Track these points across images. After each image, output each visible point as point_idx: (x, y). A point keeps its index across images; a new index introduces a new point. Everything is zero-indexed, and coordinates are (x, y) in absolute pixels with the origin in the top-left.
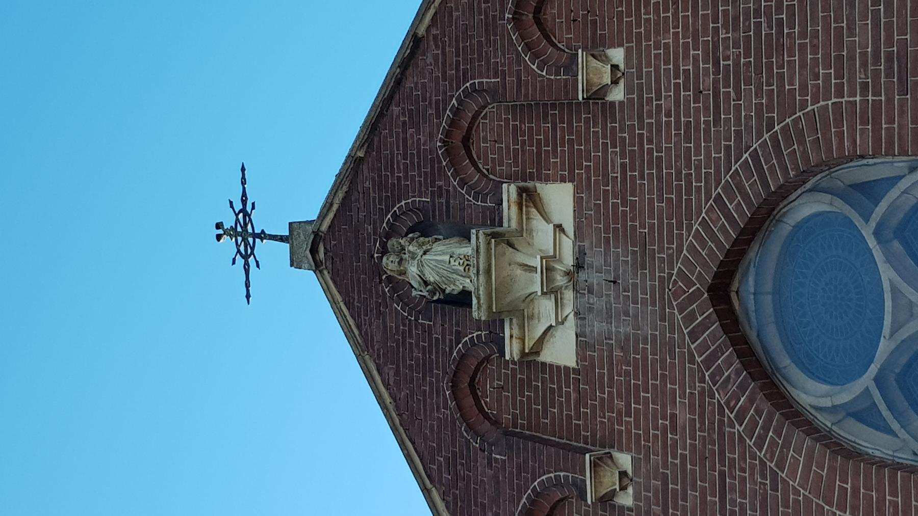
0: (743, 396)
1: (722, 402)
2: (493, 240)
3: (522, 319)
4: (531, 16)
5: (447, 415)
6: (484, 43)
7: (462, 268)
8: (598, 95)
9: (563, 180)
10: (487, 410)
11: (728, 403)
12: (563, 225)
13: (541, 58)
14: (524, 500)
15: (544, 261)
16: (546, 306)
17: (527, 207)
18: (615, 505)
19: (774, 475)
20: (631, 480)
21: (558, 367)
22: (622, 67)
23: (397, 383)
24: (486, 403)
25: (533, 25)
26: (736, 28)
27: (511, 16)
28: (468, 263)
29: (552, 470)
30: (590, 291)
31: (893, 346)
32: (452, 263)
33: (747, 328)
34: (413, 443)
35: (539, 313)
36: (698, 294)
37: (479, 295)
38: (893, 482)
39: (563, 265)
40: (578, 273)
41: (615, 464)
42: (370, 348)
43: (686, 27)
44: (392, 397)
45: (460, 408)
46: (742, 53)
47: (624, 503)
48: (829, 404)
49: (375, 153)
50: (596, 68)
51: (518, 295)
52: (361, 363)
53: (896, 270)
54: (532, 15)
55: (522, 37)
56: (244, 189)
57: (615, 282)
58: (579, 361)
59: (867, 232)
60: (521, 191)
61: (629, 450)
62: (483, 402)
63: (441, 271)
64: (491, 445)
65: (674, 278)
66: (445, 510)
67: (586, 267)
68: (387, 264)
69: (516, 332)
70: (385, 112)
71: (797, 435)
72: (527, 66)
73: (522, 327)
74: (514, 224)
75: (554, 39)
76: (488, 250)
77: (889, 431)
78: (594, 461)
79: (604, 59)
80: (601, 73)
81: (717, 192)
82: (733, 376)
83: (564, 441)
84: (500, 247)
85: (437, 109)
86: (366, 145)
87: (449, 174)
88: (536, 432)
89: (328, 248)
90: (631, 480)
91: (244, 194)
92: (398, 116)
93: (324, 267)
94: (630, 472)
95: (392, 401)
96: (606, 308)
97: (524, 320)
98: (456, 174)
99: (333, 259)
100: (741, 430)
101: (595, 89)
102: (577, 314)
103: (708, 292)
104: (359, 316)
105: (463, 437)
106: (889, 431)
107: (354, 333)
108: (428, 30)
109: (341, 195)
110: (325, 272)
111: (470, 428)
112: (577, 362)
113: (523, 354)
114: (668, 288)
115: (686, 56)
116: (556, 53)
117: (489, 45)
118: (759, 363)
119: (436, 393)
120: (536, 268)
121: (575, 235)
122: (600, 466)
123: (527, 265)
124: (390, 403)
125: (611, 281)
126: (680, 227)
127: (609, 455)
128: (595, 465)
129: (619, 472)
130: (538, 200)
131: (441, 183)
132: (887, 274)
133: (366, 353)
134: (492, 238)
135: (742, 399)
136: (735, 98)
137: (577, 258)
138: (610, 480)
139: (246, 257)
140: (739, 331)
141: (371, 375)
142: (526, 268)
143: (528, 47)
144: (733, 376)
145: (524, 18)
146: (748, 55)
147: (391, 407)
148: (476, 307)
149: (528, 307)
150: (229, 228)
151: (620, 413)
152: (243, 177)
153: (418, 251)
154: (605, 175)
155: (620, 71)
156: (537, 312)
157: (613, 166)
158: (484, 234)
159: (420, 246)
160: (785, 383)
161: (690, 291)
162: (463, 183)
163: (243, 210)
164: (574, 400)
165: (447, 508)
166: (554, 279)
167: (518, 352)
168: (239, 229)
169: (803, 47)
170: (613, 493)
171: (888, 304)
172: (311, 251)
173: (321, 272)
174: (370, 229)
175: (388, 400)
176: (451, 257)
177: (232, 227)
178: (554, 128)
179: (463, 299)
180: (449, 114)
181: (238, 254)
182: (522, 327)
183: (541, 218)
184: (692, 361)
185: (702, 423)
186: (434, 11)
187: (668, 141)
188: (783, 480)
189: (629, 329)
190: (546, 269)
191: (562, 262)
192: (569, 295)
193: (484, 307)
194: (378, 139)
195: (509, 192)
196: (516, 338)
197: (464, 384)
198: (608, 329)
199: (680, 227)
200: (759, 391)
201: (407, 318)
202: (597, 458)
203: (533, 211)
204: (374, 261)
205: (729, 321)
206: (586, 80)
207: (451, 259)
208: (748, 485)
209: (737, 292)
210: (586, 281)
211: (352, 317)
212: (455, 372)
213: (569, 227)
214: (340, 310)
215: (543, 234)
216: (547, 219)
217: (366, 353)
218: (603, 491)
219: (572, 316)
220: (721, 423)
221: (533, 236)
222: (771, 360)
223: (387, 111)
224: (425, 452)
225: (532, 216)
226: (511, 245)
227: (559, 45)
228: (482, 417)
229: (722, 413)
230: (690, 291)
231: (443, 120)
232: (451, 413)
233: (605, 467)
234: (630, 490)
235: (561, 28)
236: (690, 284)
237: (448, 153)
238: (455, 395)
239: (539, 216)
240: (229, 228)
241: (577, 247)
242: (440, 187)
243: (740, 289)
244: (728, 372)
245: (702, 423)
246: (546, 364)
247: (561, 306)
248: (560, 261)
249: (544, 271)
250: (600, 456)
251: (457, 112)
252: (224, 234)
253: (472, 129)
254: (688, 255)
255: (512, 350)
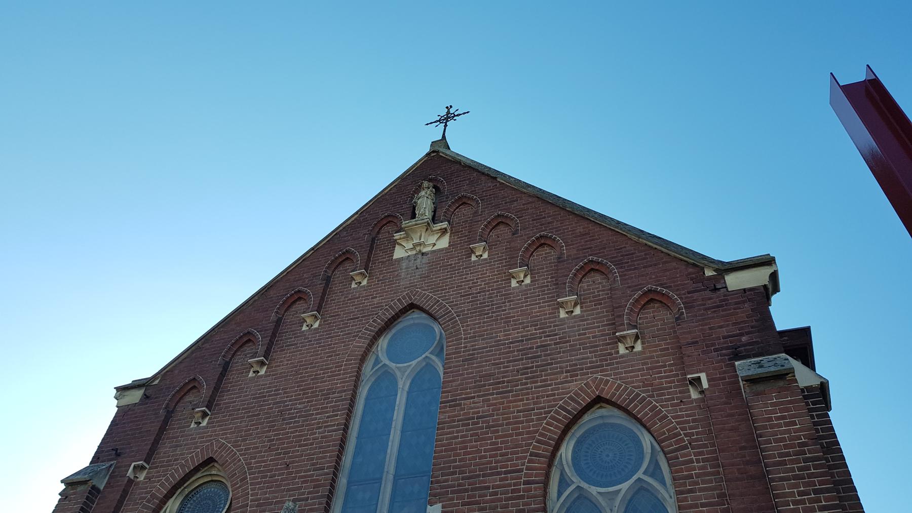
4: (500, 220)
7: (421, 213)
8: (472, 251)
9: (450, 243)
14: (353, 249)
16: (409, 245)
19: (357, 336)
22: (482, 258)
23: (391, 194)
26: (489, 298)
30: (415, 260)
31: (394, 368)
33: (403, 317)
36: (411, 299)
38: (352, 376)
43: (491, 279)
48: (379, 349)
53: (415, 365)
55: (492, 220)
57: (417, 268)
59: (427, 354)
60: (445, 229)
64: (370, 234)
69: (402, 236)
71: (367, 341)
73: (404, 238)
74: (434, 229)
76: (423, 223)
77: (372, 369)
94: (361, 285)
102: (409, 256)
106: (372, 369)
109: (450, 158)
113: (396, 240)
115: (482, 281)
126: (431, 289)
132: (414, 363)
139: (439, 121)
147: (383, 193)
151: (378, 278)
152: (465, 113)
154: (449, 258)
160: (384, 336)
163: (455, 116)
171: (406, 365)
172: (433, 151)
179: (413, 216)
182: (404, 238)
184: (392, 301)
185: (374, 308)
188: (355, 339)
189: (403, 276)
192: (414, 252)
195: (445, 225)
199: (431, 289)
209: (413, 312)
213: (435, 248)
214: (414, 167)
215: (432, 239)
216: (436, 241)
218: (354, 277)
220: (373, 314)
222: (395, 326)
226: (427, 230)
234: (356, 286)
235: (496, 232)
245: (374, 308)
248: (424, 247)
251: (472, 199)
255: (397, 236)
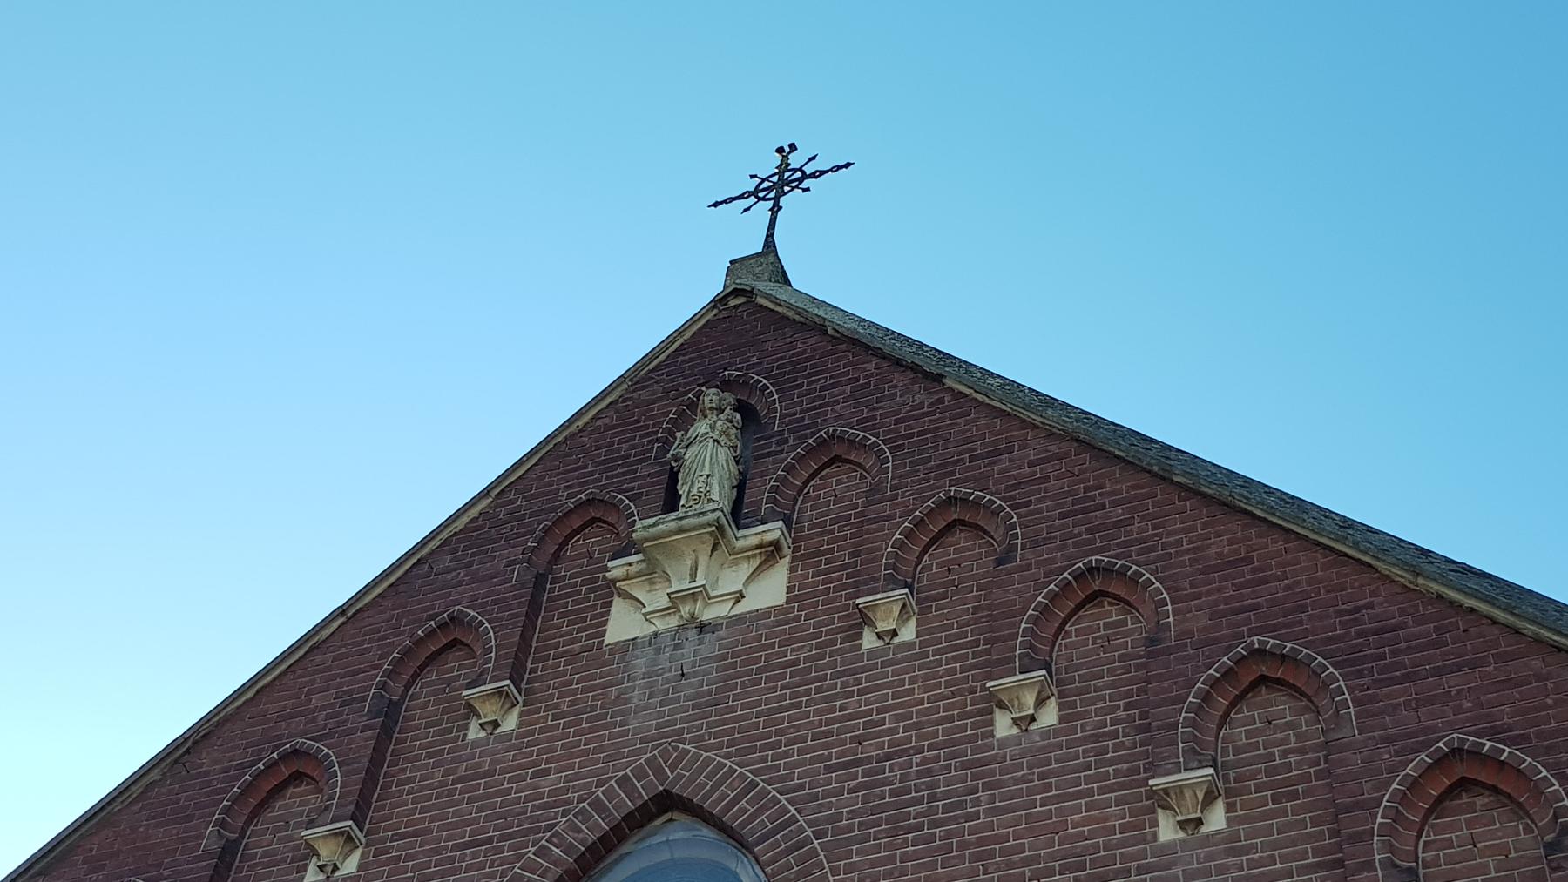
0: (561, 851)
1: (557, 828)
2: (714, 528)
3: (648, 572)
4: (956, 516)
5: (561, 501)
6: (929, 465)
7: (695, 491)
9: (790, 590)
10: (571, 543)
11: (557, 834)
12: (744, 599)
13: (906, 541)
15: (701, 589)
17: (760, 553)
18: (469, 719)
20: (491, 734)
21: (605, 623)
22: (896, 640)
23: (597, 431)
24: (578, 540)
25: (945, 521)
26: (920, 775)
27: (952, 494)
28: (703, 497)
29: (498, 642)
32: (701, 479)
33: (635, 839)
34: (536, 464)
35: (656, 590)
37: (658, 525)
39: (702, 608)
40: (696, 627)
41: (505, 713)
42: (635, 387)
44: (584, 426)
45: (567, 514)
46: (895, 786)
47: (471, 729)
49: (830, 348)
50: (891, 612)
51: (666, 566)
52: (315, 630)
54: (957, 518)
56: (827, 172)
57: (683, 675)
58: (610, 647)
60: (776, 544)
61: (520, 725)
62: (579, 536)
63: (695, 466)
65: (681, 746)
66: (470, 518)
67: (700, 636)
68: (709, 395)
69: (634, 569)
70: (870, 352)
72: (899, 524)
73: (640, 574)
74: (740, 544)
75: (932, 549)
76: (702, 526)
78: (502, 691)
79: (905, 617)
80: (888, 617)
81: (760, 782)
82: (581, 836)
83: (534, 645)
84: (708, 537)
85: (867, 419)
86: (839, 336)
87: (799, 450)
88: (545, 608)
89: (740, 309)
90: (491, 734)
91: (823, 173)
92: (865, 370)
93: (721, 308)
94: (499, 731)
95: (580, 427)
96: (659, 669)
97: (647, 575)
98: (799, 458)
99: (728, 317)
100: (530, 855)
101: (870, 614)
102: (656, 634)
103: (664, 790)
104: (667, 366)
105: (539, 524)
107: (650, 363)
108: (951, 389)
109: (790, 314)
110: (715, 312)
111: (547, 530)
112: (609, 645)
113: (614, 581)
114: (672, 741)
115: (898, 718)
116: (914, 558)
117: (926, 472)
118: (600, 859)
119: (584, 482)
120: (695, 581)
121: (734, 616)
122: (501, 697)
123: (696, 569)
124: (578, 426)
125: (682, 670)
127: (515, 702)
128: (500, 693)
129: (496, 720)
130: (771, 563)
131: (791, 442)
133: (630, 383)
134: (717, 527)
135: (558, 851)
136: (851, 786)
137: (710, 623)
138: (489, 711)
140: (631, 830)
141: (605, 396)
142: (694, 569)
143: (919, 523)
144: (581, 836)
145: (953, 509)
146: (893, 794)
147: (573, 428)
148: (646, 524)
149: (660, 577)
150: (789, 162)
151: (556, 706)
153: (717, 432)
154: (789, 642)
155: (892, 639)
156: (657, 587)
157: (799, 649)
158: (718, 518)
159: (724, 433)
161: (666, 768)
162: (790, 469)
163: (805, 176)
164: (573, 648)
165: (471, 521)
166: (685, 603)
167: (614, 576)
168: (787, 175)
169: (891, 860)
170: (479, 716)
172: (735, 289)
173: (714, 307)
174: (754, 360)
175: (580, 423)
176: (708, 476)
177: (789, 164)
178: (844, 568)
180: (861, 436)
181: (760, 180)
182: (640, 574)
183: (751, 572)
184: (600, 784)
186: (968, 393)
187: (818, 713)
190: (693, 593)
191: (706, 606)
192: (673, 622)
193: (645, 534)
194: (845, 349)
195: (773, 530)
196: (628, 570)
197: (593, 513)
198: (638, 676)
200: (564, 868)
201: (660, 428)
202: (507, 693)
203: (757, 561)
204: (720, 373)
205: (639, 817)
206: (877, 604)
207: (705, 477)
208: (476, 873)
209: (671, 820)
210: (687, 640)
211: (668, 356)
212: (602, 501)
215: (733, 579)
217: (630, 383)
219: (654, 629)
220: (537, 830)
221: (731, 567)
223: (871, 354)
224: (527, 480)
225: (751, 560)
226: (714, 548)
227: (926, 557)
228: (561, 540)
229: (549, 828)
230: (666, 768)
231: (855, 429)
232: (562, 505)
233: (500, 704)
234: (482, 734)
236: (673, 768)
237: (823, 443)
238: (581, 505)
239: (752, 570)
240: (789, 162)
241: (721, 621)
242: (787, 441)
243: (675, 822)
244: (585, 829)
246: (610, 607)
247: (662, 615)
248: (707, 605)
249: (691, 592)
250: (510, 694)
252: (783, 156)
253: (850, 463)
254: (701, 759)
255: (617, 568)
